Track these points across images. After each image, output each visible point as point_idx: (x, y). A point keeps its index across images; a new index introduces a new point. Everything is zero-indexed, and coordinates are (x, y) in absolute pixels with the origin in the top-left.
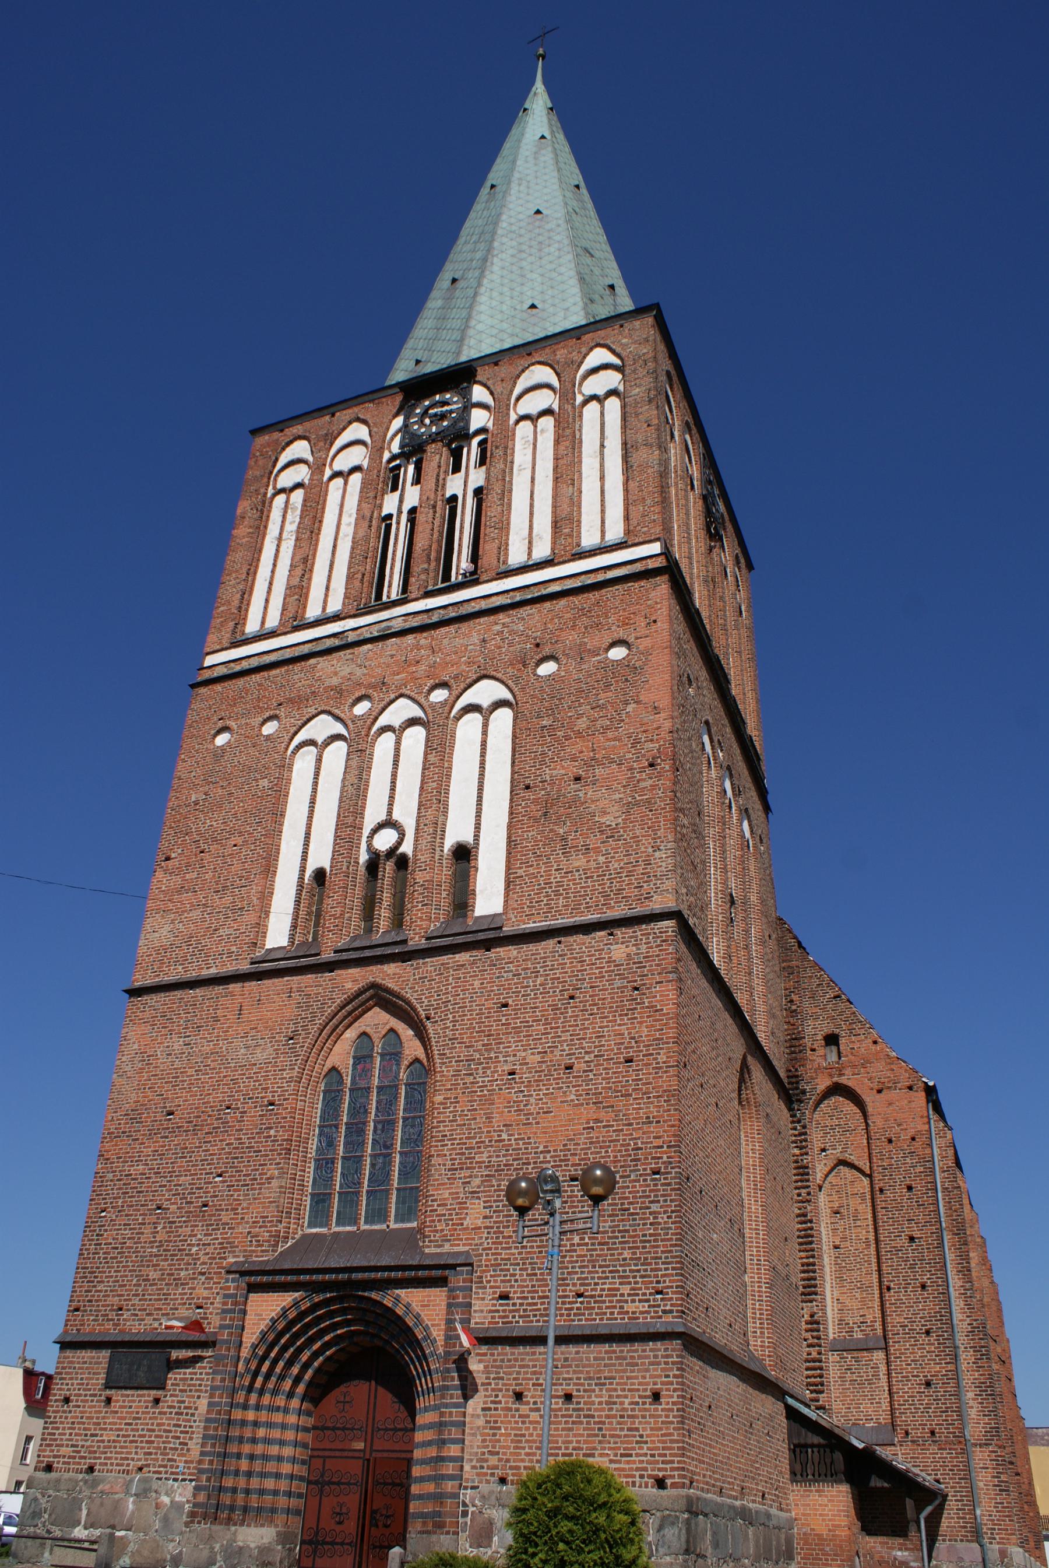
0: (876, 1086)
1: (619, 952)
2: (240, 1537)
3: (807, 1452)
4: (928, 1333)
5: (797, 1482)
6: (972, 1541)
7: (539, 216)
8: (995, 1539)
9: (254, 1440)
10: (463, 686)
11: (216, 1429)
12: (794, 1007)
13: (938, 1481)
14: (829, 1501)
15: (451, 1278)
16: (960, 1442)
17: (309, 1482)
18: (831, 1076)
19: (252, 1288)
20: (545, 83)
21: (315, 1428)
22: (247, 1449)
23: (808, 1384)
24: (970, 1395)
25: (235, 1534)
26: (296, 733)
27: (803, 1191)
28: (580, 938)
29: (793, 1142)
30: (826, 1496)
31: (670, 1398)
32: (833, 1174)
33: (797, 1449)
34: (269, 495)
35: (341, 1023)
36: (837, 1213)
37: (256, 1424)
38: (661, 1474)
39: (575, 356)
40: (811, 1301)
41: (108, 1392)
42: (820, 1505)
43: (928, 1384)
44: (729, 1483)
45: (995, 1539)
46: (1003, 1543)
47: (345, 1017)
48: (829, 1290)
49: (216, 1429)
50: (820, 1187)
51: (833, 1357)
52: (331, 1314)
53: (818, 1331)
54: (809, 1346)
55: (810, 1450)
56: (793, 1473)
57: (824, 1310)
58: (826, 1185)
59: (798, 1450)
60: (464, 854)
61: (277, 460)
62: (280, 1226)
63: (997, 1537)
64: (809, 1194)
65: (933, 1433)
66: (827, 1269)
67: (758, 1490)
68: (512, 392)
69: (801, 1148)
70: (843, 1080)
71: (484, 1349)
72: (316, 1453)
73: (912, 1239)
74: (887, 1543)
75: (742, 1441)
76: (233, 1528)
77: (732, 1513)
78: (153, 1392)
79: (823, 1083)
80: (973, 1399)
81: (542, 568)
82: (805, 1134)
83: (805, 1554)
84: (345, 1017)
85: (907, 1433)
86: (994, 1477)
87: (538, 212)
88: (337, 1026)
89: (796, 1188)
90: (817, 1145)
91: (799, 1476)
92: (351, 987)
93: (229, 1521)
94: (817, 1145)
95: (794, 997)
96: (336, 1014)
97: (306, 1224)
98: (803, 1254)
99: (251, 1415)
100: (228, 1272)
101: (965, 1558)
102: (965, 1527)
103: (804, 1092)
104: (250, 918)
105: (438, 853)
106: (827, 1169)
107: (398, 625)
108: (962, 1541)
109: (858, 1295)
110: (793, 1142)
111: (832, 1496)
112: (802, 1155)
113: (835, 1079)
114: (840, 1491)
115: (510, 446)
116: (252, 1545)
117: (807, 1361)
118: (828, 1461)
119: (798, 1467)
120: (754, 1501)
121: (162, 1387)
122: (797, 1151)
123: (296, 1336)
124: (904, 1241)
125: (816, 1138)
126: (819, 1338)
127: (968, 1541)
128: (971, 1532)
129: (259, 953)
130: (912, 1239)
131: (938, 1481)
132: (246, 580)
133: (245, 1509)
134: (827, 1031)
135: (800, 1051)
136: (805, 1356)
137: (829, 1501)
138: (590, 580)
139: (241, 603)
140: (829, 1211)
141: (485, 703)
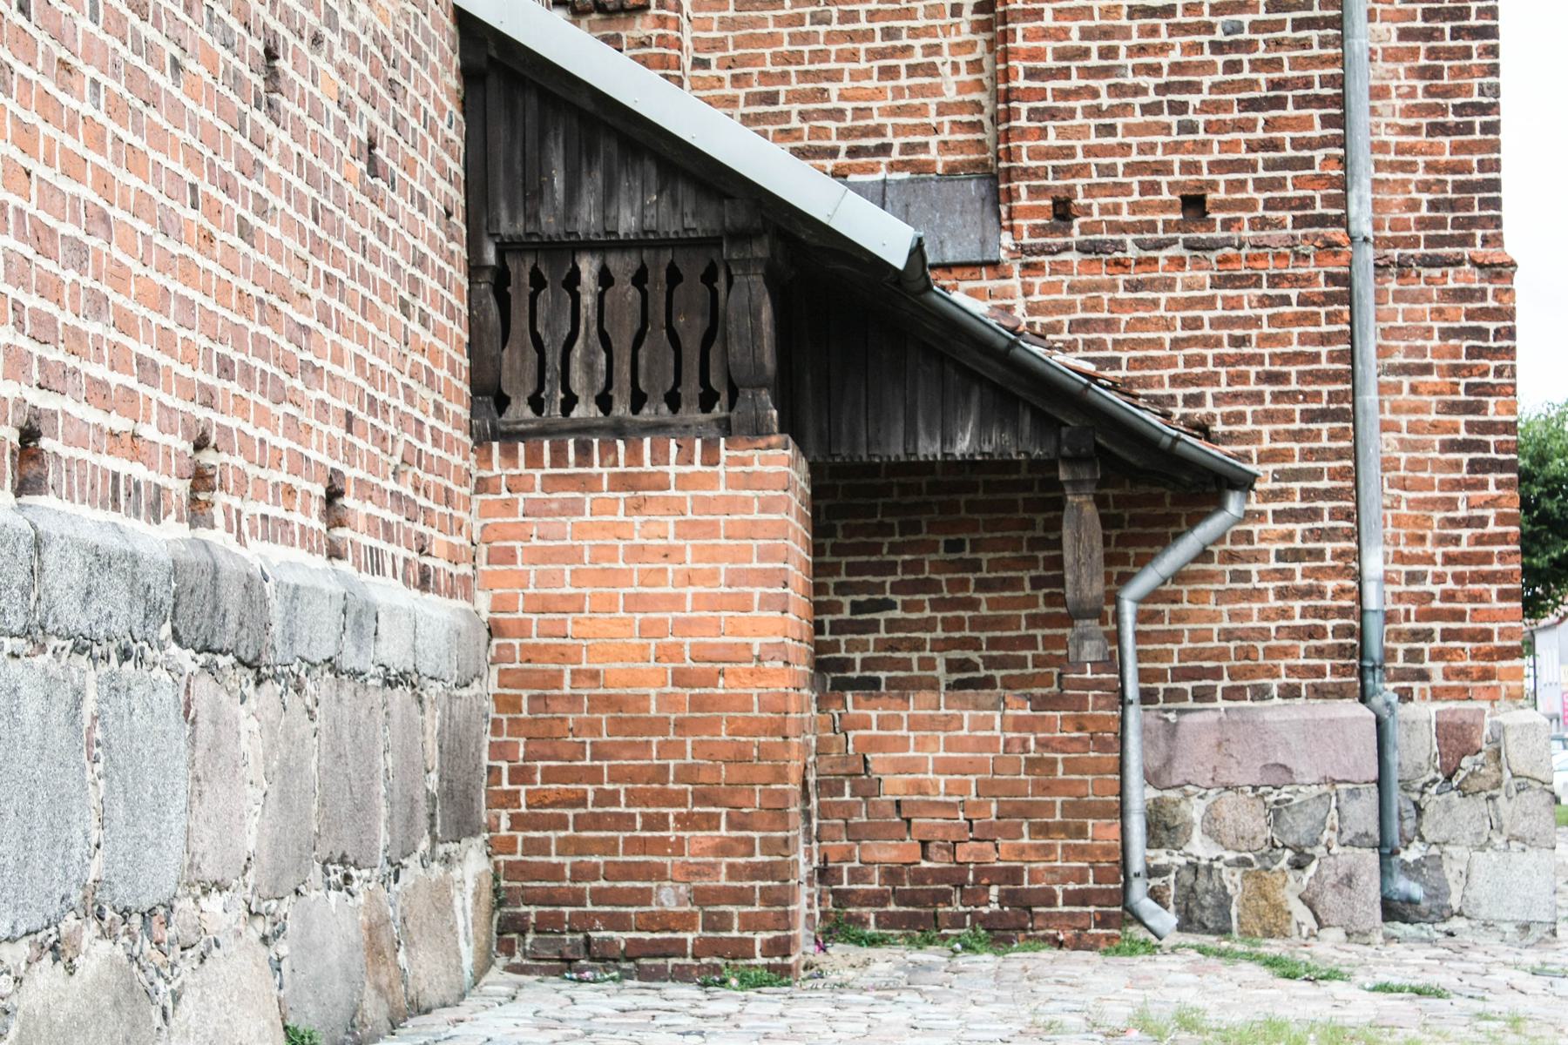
3: (574, 278)
5: (509, 437)
6: (1340, 692)
8: (1423, 676)
14: (685, 529)
15: (149, 580)
16: (1330, 246)
30: (675, 507)
33: (511, 276)
42: (636, 553)
44: (98, 393)
45: (1423, 676)
46: (1464, 695)
55: (588, 267)
56: (488, 393)
59: (521, 270)
63: (1436, 668)
65: (1194, 204)
67: (300, 464)
74: (948, 723)
75: (209, 135)
77: (118, 612)
80: (1392, 55)
83: (537, 800)
85: (1063, 211)
86: (1452, 408)
91: (520, 411)
101: (1299, 766)
102: (1313, 633)
108: (1290, 692)
111: (704, 505)
118: (691, 328)
119: (516, 366)
120: (273, 530)
127: (1319, 692)
128: (1341, 651)
137: (685, 529)
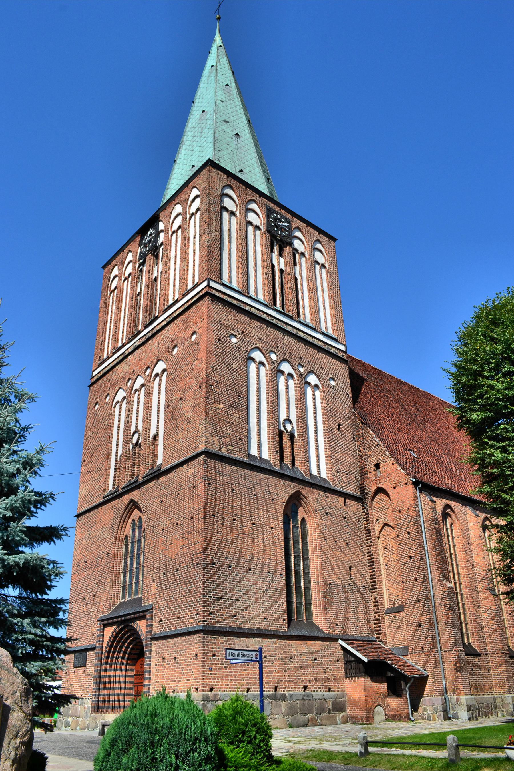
0: (393, 486)
1: (190, 472)
2: (106, 718)
4: (419, 601)
7: (204, 113)
9: (110, 683)
10: (153, 366)
11: (96, 680)
12: (361, 454)
13: (425, 670)
17: (134, 696)
18: (376, 484)
19: (105, 626)
20: (220, 33)
21: (135, 675)
22: (107, 686)
23: (375, 631)
24: (444, 628)
25: (104, 717)
26: (114, 399)
27: (369, 541)
28: (180, 469)
29: (364, 518)
31: (200, 656)
32: (383, 530)
33: (347, 663)
34: (108, 295)
35: (126, 517)
36: (386, 548)
37: (110, 676)
38: (197, 687)
39: (187, 197)
40: (374, 592)
41: (75, 669)
43: (420, 625)
47: (127, 514)
48: (385, 587)
49: (96, 680)
50: (378, 538)
51: (386, 617)
52: (124, 635)
53: (378, 605)
54: (375, 613)
57: (382, 596)
58: (381, 536)
60: (155, 437)
61: (110, 278)
62: (111, 601)
64: (371, 542)
65: (423, 648)
66: (383, 576)
68: (169, 221)
69: (367, 521)
70: (381, 486)
71: (155, 642)
72: (136, 685)
73: (411, 557)
76: (103, 715)
78: (84, 668)
79: (373, 488)
80: (445, 630)
81: (175, 304)
82: (368, 514)
84: (127, 514)
86: (454, 665)
87: (204, 111)
88: (125, 519)
89: (366, 540)
90: (375, 518)
92: (126, 502)
93: (102, 712)
94: (375, 518)
95: (361, 449)
96: (123, 514)
97: (121, 599)
98: (370, 571)
99: (108, 673)
100: (98, 621)
103: (367, 494)
104: (103, 480)
105: (148, 441)
106: (380, 529)
107: (138, 343)
109: (395, 587)
110: (364, 518)
112: (367, 524)
113: (378, 486)
114: (361, 681)
115: (169, 248)
116: (110, 720)
117: (374, 620)
121: (85, 666)
122: (365, 523)
123: (118, 642)
124: (407, 559)
125: (374, 514)
126: (378, 609)
129: (107, 493)
130: (411, 557)
131: (425, 670)
132: (102, 336)
133: (108, 708)
134: (375, 462)
135: (365, 474)
136: (373, 618)
138: (186, 306)
139: (101, 346)
140: (383, 548)
141: (159, 372)
